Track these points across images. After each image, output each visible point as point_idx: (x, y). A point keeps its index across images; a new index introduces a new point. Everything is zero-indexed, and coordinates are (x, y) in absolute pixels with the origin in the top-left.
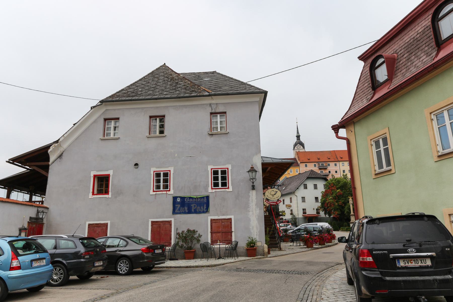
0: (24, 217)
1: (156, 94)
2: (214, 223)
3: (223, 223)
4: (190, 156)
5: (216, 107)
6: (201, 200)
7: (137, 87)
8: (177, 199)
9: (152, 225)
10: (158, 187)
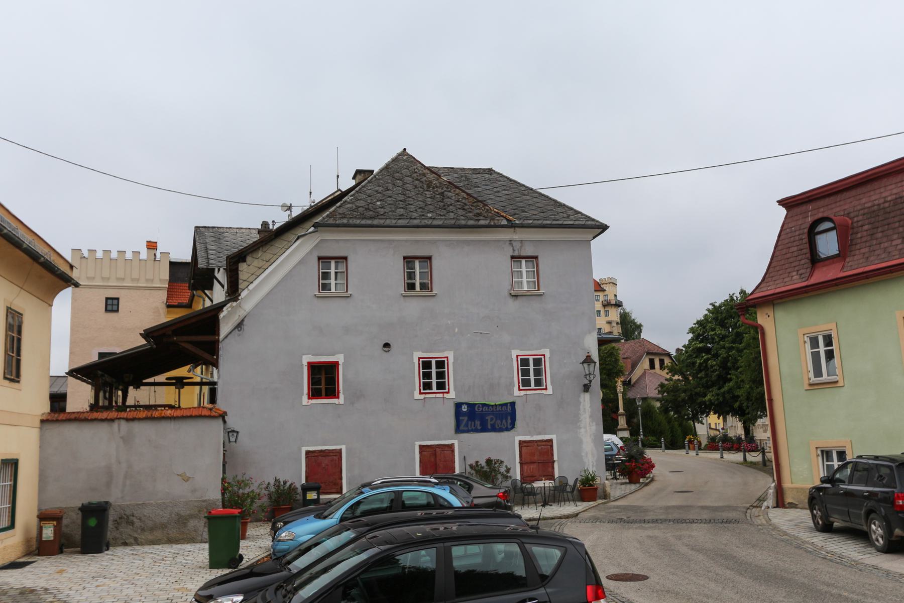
1: (414, 217)
2: (525, 448)
3: (540, 448)
4: (481, 333)
5: (521, 247)
6: (502, 408)
8: (461, 407)
9: (420, 453)
10: (428, 386)
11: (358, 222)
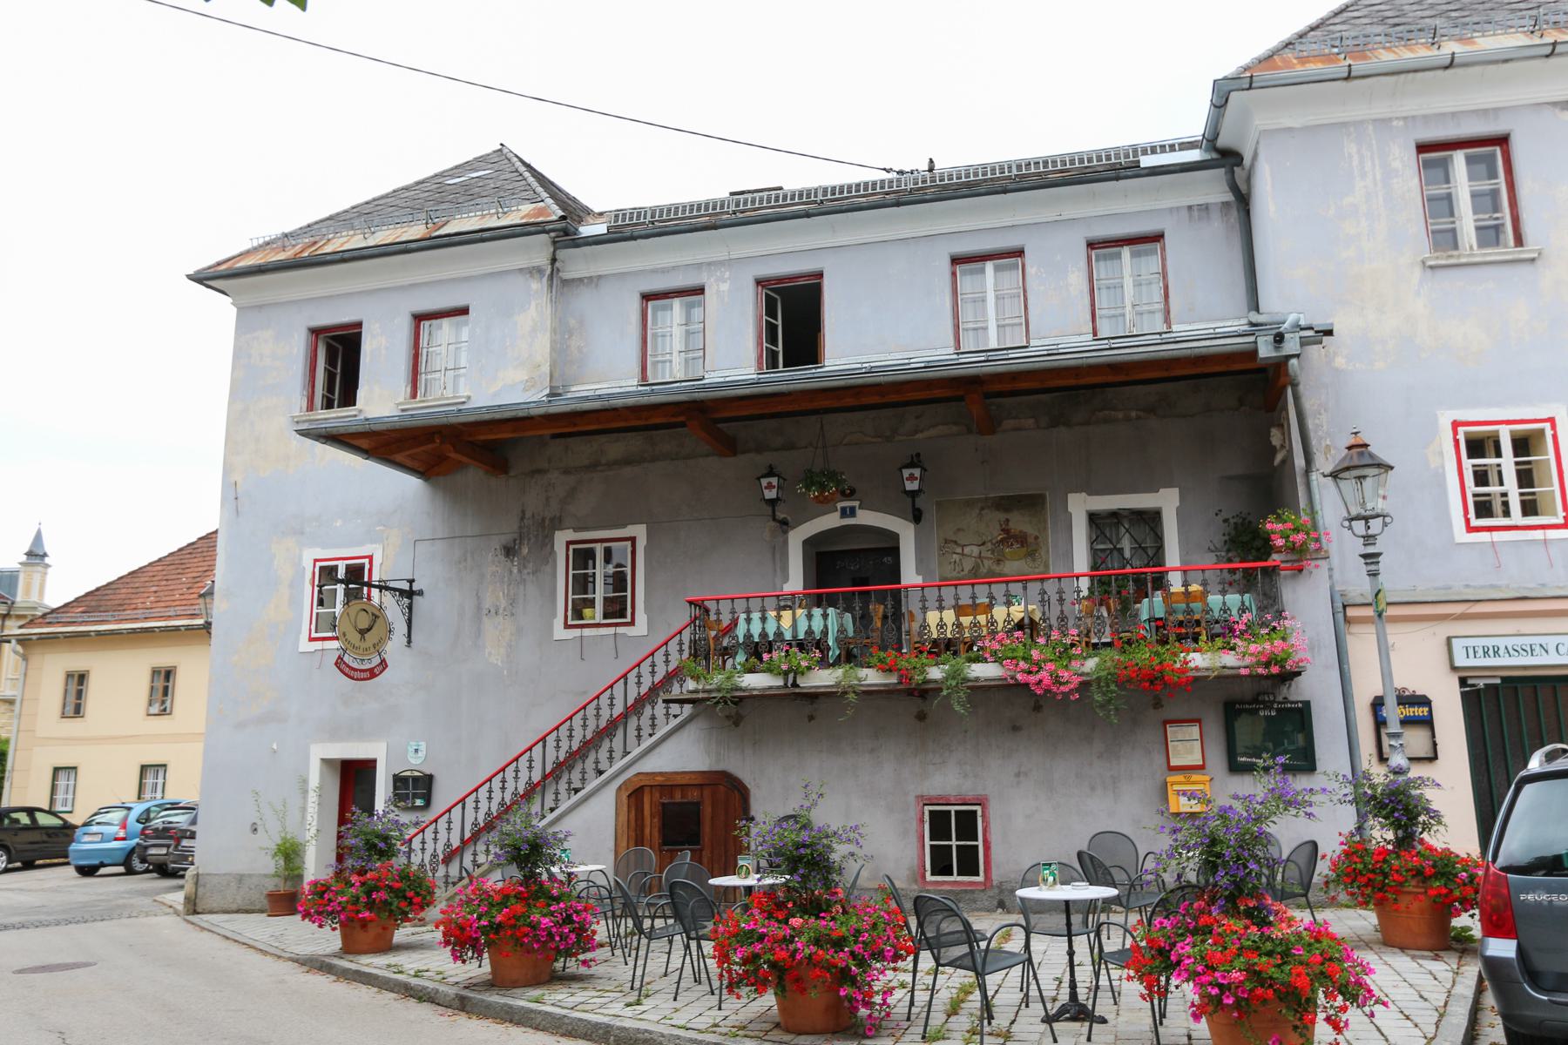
0: (275, 747)
10: (1446, 239)
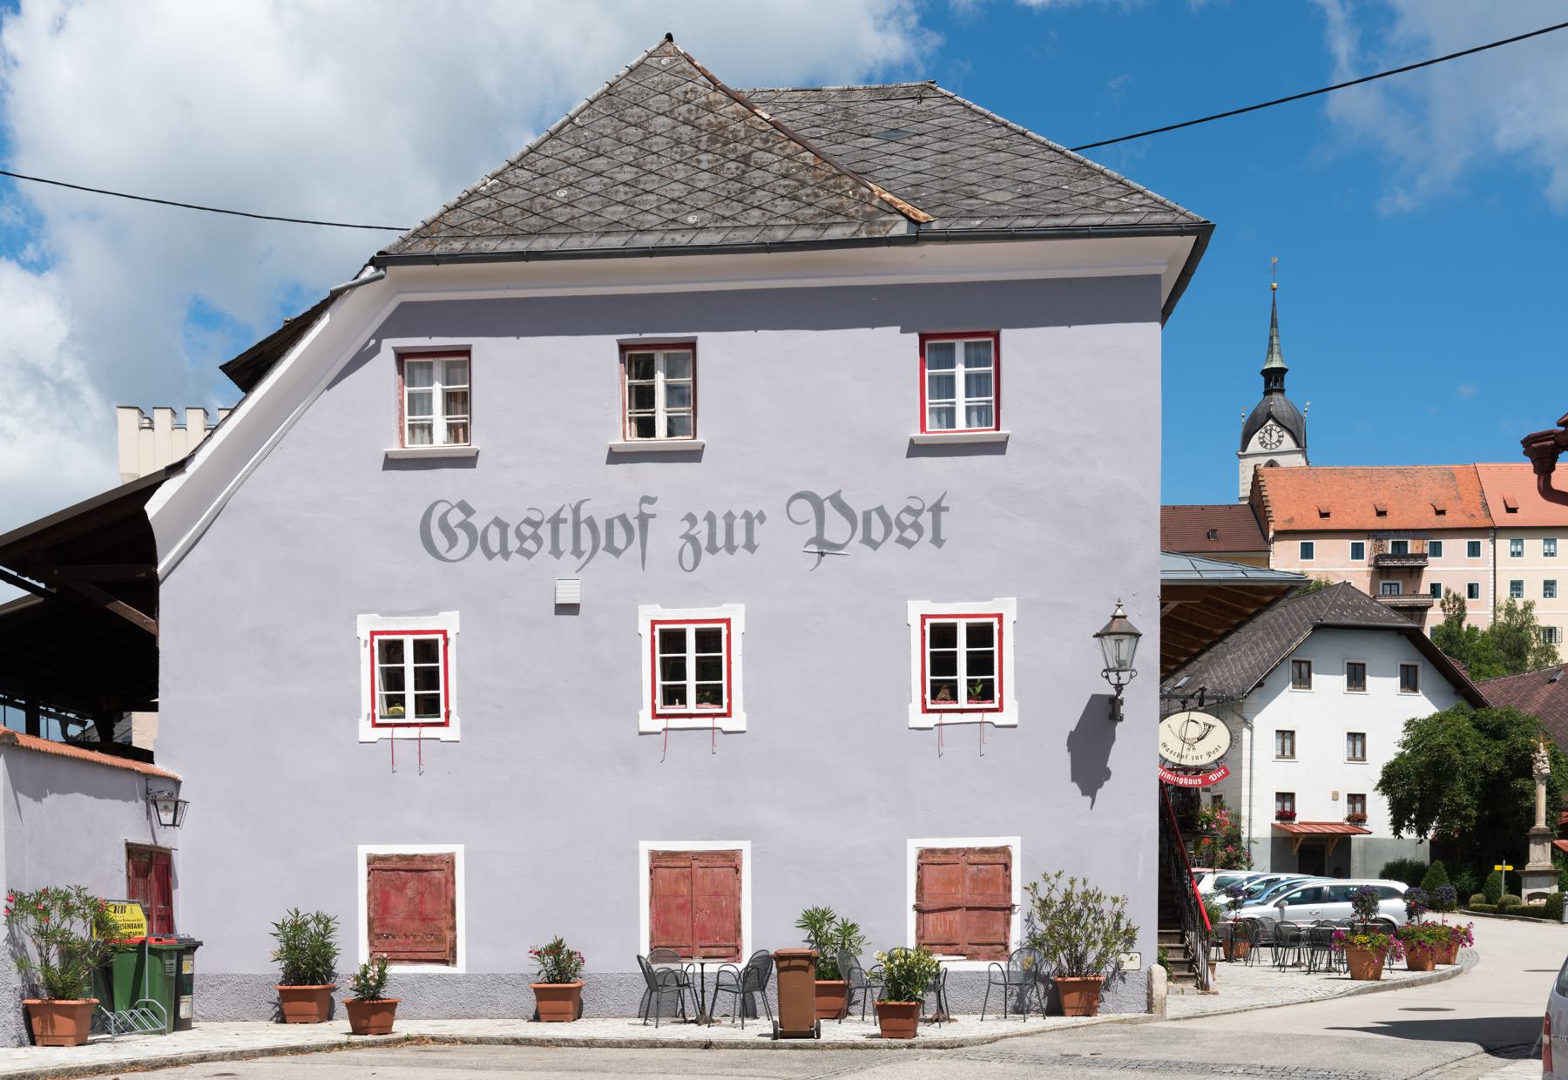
1: (648, 226)
7: (545, 179)
11: (490, 246)
